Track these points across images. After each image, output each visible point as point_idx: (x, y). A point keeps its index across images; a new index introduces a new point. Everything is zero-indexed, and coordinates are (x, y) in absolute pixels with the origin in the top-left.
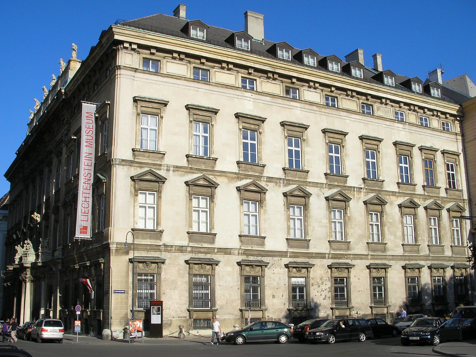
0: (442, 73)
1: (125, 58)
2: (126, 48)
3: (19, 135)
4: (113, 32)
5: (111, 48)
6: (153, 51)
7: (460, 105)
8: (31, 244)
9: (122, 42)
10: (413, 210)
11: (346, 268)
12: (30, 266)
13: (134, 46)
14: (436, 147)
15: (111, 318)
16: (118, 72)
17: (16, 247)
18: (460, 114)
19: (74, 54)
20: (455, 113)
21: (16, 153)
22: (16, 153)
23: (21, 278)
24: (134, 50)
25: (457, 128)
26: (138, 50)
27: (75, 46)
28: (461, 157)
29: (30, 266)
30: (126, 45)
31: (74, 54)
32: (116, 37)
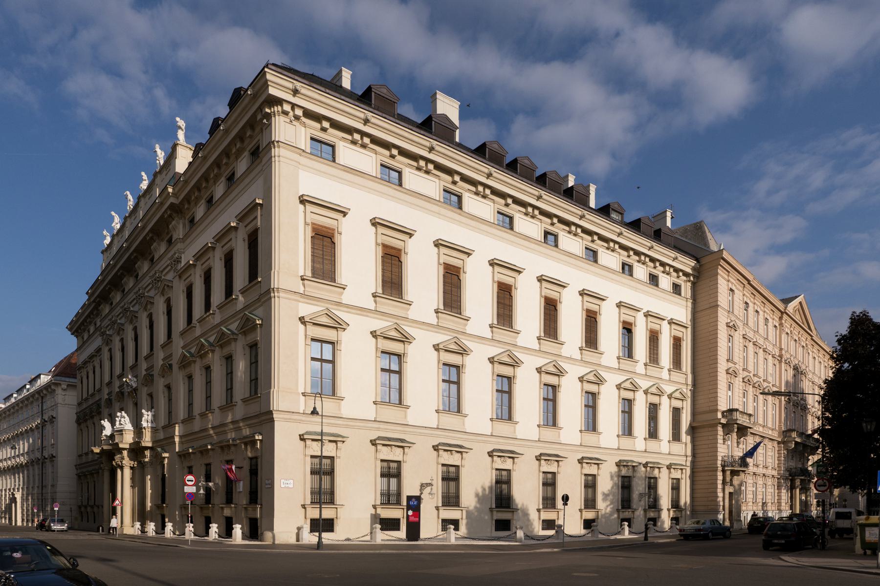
0: (672, 218)
1: (287, 131)
2: (286, 113)
3: (91, 270)
4: (267, 81)
5: (261, 111)
6: (326, 124)
7: (697, 260)
8: (127, 419)
9: (279, 101)
10: (632, 393)
11: (510, 457)
12: (128, 446)
13: (299, 112)
14: (662, 313)
15: (348, 540)
16: (275, 151)
17: (102, 422)
18: (696, 274)
19: (181, 135)
20: (689, 271)
21: (87, 293)
22: (87, 293)
23: (114, 463)
24: (297, 118)
25: (686, 289)
26: (303, 119)
27: (181, 123)
28: (689, 330)
29: (128, 446)
30: (287, 107)
31: (181, 135)
32: (272, 91)
